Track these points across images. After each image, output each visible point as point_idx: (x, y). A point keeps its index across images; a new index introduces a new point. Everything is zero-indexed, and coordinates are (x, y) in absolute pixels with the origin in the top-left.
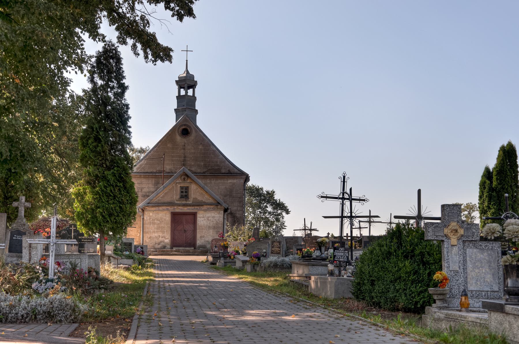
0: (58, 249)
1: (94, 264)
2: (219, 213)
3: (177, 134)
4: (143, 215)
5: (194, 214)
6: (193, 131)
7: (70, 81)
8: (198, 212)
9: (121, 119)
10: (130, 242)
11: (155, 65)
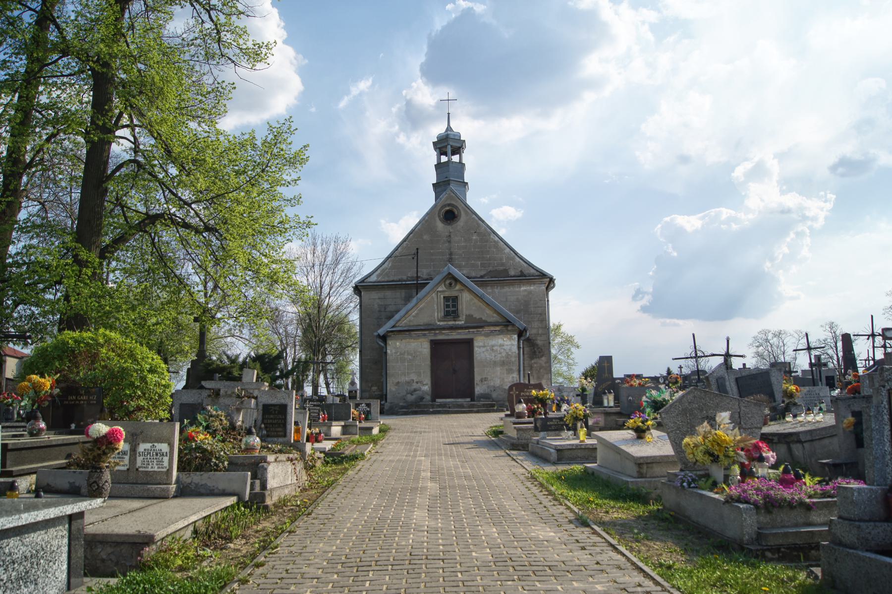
2: (510, 339)
3: (437, 219)
6: (462, 213)
8: (475, 339)
10: (283, 401)
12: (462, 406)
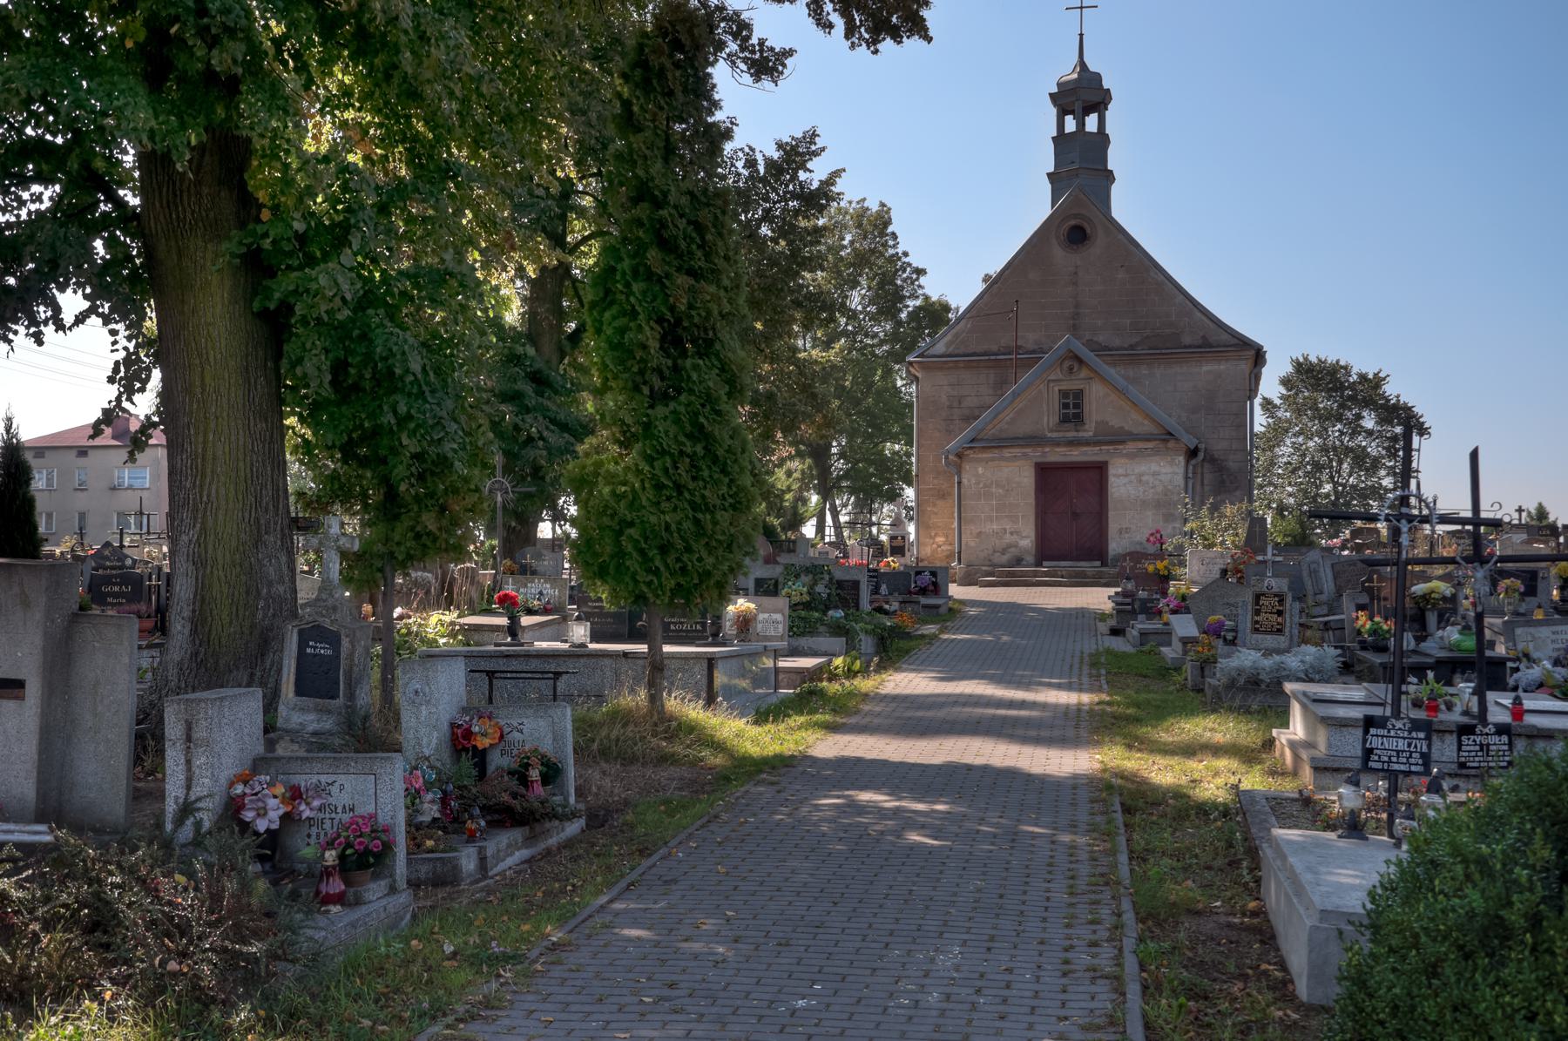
0: (427, 689)
1: (550, 735)
4: (959, 474)
5: (1101, 468)
7: (732, 123)
9: (703, 238)
10: (855, 578)
11: (876, 52)
12: (1082, 575)
